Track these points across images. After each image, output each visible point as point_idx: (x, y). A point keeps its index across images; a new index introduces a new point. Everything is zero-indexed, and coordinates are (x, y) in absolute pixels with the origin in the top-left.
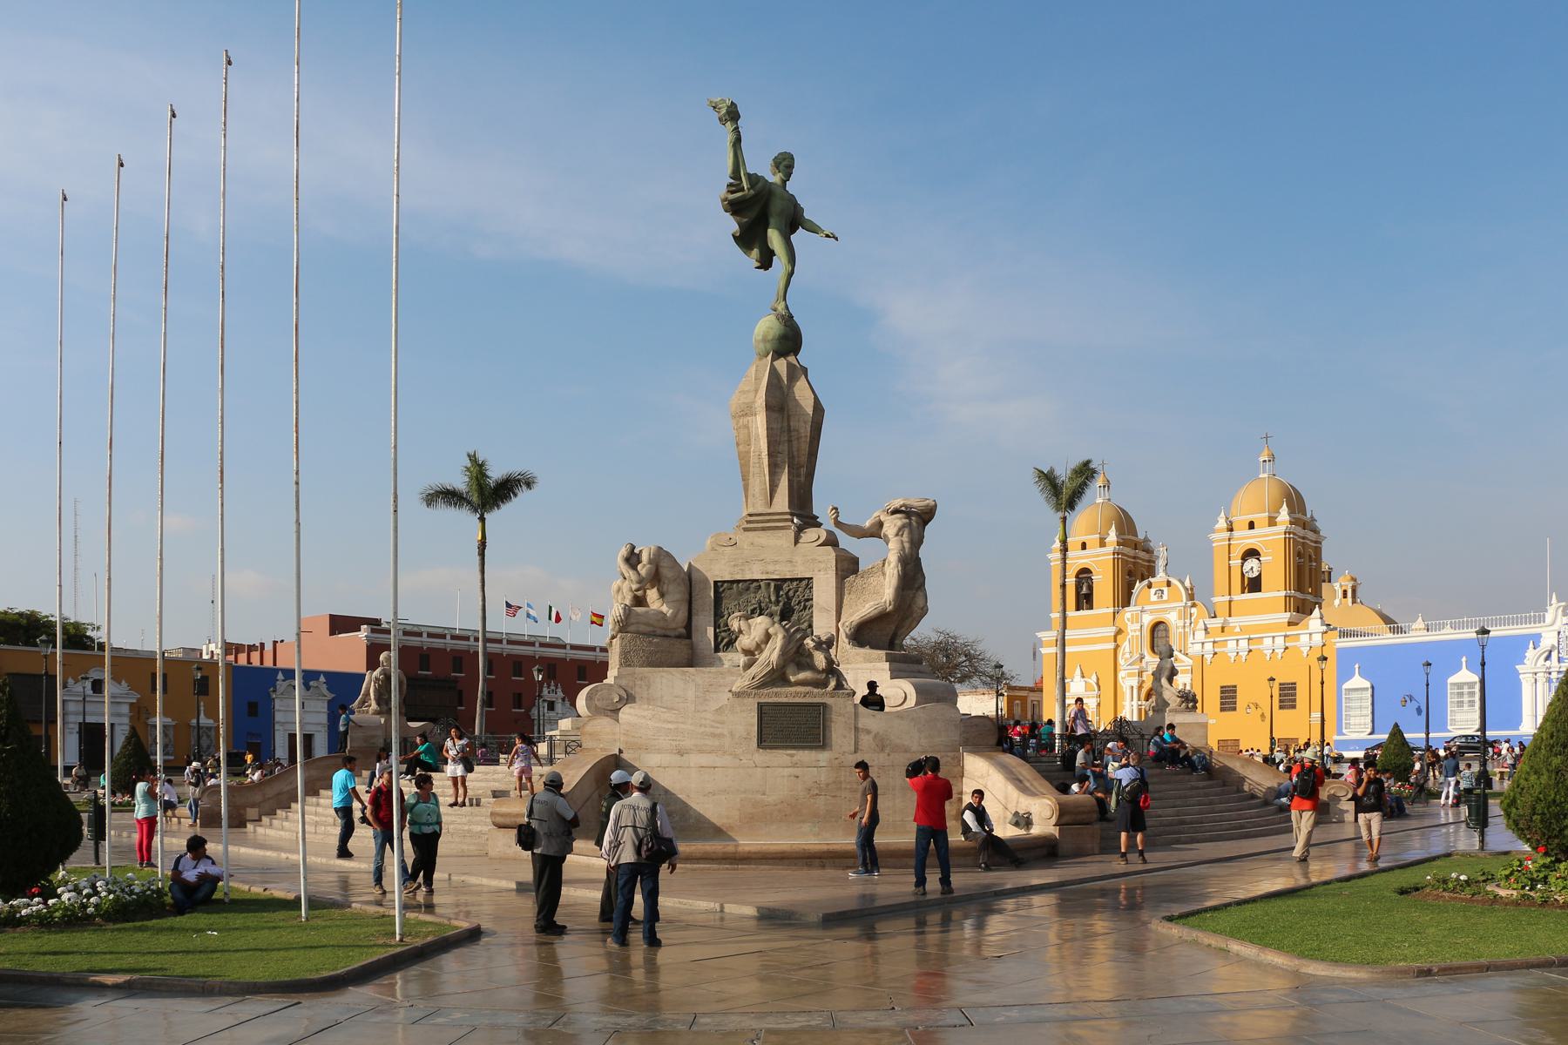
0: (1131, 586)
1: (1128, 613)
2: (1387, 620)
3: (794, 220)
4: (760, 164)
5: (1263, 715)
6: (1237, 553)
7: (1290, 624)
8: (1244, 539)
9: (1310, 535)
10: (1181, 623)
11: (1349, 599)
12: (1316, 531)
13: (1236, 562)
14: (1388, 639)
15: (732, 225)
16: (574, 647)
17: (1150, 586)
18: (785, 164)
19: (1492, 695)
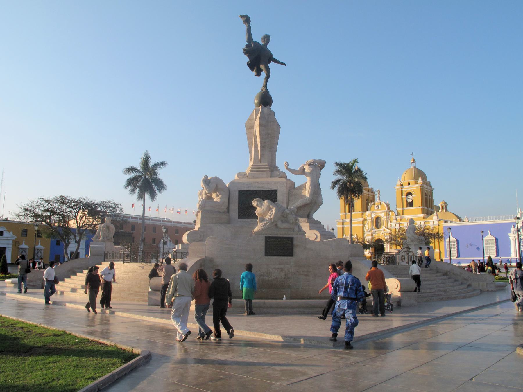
0: (368, 204)
1: (367, 214)
2: (458, 217)
3: (270, 58)
4: (257, 38)
5: (478, 248)
6: (404, 193)
7: (424, 218)
8: (407, 189)
9: (429, 188)
10: (386, 217)
11: (444, 210)
12: (430, 186)
13: (404, 196)
14: (459, 224)
15: (247, 59)
16: (174, 222)
17: (374, 204)
18: (267, 38)
19: (500, 245)
